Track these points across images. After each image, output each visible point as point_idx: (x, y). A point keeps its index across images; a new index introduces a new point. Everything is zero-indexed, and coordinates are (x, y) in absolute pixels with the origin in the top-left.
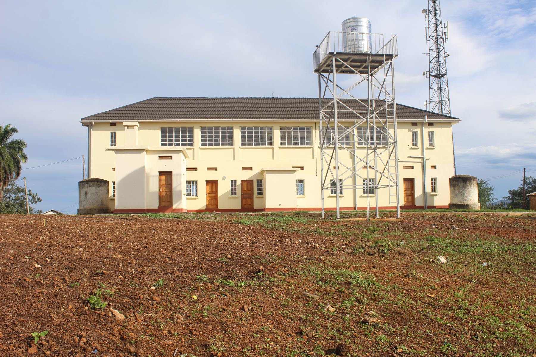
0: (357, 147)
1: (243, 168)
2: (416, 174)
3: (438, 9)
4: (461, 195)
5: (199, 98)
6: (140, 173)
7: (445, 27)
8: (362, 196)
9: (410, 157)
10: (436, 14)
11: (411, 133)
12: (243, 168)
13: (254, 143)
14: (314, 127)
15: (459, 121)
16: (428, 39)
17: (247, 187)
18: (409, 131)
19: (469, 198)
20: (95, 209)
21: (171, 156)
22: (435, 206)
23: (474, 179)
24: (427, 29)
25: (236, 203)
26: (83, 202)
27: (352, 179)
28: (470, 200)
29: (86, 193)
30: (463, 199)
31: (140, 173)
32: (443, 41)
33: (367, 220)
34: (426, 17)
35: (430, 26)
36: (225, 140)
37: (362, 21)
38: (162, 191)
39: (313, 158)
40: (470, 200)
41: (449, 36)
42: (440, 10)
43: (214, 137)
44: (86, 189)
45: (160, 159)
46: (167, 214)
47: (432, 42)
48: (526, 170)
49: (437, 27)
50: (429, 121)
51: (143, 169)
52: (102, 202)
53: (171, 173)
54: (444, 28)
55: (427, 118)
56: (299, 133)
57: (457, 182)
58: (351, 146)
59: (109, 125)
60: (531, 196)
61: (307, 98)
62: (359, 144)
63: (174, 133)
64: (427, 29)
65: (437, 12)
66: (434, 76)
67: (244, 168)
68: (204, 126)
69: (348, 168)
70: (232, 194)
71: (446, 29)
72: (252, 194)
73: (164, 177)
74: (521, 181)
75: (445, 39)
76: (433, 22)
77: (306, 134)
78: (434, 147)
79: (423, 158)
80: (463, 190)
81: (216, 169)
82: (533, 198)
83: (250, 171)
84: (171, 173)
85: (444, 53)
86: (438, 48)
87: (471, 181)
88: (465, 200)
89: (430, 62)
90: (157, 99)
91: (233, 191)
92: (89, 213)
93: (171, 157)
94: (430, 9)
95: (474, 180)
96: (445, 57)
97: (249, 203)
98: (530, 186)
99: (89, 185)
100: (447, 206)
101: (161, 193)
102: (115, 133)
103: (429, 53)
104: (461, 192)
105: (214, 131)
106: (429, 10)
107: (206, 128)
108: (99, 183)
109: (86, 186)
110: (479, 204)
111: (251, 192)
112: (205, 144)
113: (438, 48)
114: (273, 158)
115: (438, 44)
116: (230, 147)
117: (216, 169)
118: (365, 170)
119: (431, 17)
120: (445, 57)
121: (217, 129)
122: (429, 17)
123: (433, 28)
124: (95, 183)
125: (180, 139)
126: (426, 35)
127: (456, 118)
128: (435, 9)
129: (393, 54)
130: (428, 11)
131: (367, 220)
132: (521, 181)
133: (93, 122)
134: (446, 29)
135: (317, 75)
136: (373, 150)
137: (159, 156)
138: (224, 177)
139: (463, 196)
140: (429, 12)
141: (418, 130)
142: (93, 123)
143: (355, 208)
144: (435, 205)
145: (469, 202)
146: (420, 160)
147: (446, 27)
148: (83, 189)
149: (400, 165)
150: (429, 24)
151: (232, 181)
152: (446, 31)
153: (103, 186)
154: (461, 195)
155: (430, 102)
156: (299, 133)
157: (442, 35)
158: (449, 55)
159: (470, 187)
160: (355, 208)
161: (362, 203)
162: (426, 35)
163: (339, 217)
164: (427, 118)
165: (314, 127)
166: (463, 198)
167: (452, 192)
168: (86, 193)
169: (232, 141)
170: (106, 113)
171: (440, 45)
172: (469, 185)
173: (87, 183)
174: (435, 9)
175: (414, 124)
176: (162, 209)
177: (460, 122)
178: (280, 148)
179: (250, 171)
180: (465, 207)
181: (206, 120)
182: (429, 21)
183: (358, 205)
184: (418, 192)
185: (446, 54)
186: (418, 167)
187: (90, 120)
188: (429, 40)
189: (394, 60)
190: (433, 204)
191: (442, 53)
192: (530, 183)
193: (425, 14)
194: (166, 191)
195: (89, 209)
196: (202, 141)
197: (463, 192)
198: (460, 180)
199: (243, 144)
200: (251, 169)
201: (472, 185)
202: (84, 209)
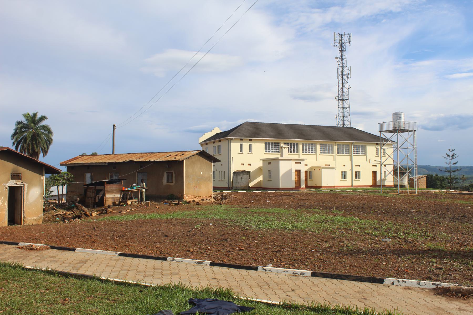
2: (377, 169)
8: (355, 180)
9: (375, 161)
10: (342, 60)
11: (376, 148)
20: (247, 187)
21: (300, 162)
24: (338, 69)
27: (351, 171)
29: (242, 178)
32: (347, 78)
39: (334, 160)
41: (351, 75)
42: (346, 58)
44: (241, 176)
47: (340, 77)
54: (348, 70)
55: (384, 142)
64: (338, 69)
66: (341, 100)
71: (350, 71)
75: (349, 77)
79: (381, 161)
85: (348, 86)
88: (404, 183)
89: (339, 91)
93: (300, 163)
96: (348, 89)
100: (393, 185)
109: (241, 174)
114: (317, 160)
116: (297, 153)
120: (348, 89)
123: (341, 69)
130: (338, 58)
133: (234, 138)
134: (350, 71)
140: (339, 59)
141: (379, 147)
143: (352, 186)
146: (379, 162)
147: (349, 69)
148: (239, 176)
150: (339, 67)
152: (350, 72)
155: (338, 116)
157: (347, 74)
158: (351, 87)
160: (352, 186)
162: (337, 73)
164: (384, 142)
168: (242, 178)
171: (344, 80)
173: (242, 173)
175: (377, 144)
184: (378, 179)
185: (349, 87)
186: (378, 165)
188: (339, 77)
191: (346, 86)
193: (337, 60)
202: (241, 187)
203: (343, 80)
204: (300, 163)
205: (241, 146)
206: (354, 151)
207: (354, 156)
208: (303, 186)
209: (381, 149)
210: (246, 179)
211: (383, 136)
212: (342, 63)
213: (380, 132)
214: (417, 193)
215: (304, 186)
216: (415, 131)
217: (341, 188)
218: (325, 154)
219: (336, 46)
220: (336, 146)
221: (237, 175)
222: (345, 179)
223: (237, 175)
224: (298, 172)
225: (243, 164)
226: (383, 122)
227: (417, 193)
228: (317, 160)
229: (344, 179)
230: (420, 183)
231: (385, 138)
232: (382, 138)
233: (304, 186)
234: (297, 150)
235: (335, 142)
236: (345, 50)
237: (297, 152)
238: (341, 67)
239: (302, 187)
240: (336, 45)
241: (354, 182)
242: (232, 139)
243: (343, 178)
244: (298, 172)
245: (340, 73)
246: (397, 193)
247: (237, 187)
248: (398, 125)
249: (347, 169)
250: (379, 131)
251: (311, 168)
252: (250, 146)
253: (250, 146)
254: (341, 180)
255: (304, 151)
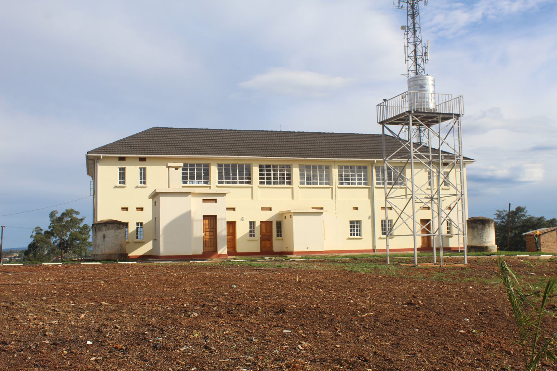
0: (375, 187)
1: (262, 208)
3: (417, 26)
4: (480, 237)
5: (203, 129)
6: (187, 217)
7: (425, 47)
8: (380, 238)
10: (415, 32)
11: (427, 172)
12: (262, 208)
13: (273, 182)
14: (333, 166)
15: (473, 162)
16: (407, 59)
17: (266, 229)
18: (426, 171)
19: (487, 240)
20: (115, 254)
21: (216, 200)
22: (451, 248)
23: (492, 221)
24: (406, 48)
25: (255, 246)
26: (100, 246)
27: (370, 220)
28: (489, 242)
29: (104, 237)
30: (482, 242)
31: (187, 217)
32: (423, 61)
33: (440, 266)
34: (405, 35)
35: (409, 44)
36: (243, 178)
37: (427, 80)
38: (206, 236)
39: (332, 198)
40: (489, 242)
41: (429, 56)
42: (420, 28)
43: (231, 174)
45: (203, 202)
46: (214, 260)
47: (411, 62)
48: (511, 206)
49: (415, 46)
50: (445, 161)
51: (189, 213)
52: (121, 246)
53: (215, 217)
54: (424, 48)
56: (318, 172)
57: (475, 224)
58: (370, 187)
59: (118, 159)
60: (529, 235)
61: (316, 133)
62: (378, 184)
63: (189, 170)
64: (406, 48)
65: (416, 29)
67: (263, 209)
68: (221, 162)
69: (409, 216)
70: (251, 236)
71: (426, 50)
72: (271, 236)
73: (207, 222)
74: (494, 214)
75: (426, 60)
76: (412, 40)
77: (325, 173)
78: (449, 188)
80: (482, 233)
81: (234, 209)
82: (529, 237)
83: (269, 212)
84: (215, 217)
86: (417, 70)
87: (489, 223)
88: (484, 242)
90: (157, 129)
91: (252, 234)
92: (95, 258)
93: (215, 201)
94: (409, 25)
95: (492, 222)
97: (268, 246)
98: (504, 221)
99: (107, 228)
101: (205, 238)
102: (124, 169)
103: (408, 75)
104: (480, 234)
105: (231, 168)
106: (408, 26)
107: (223, 165)
108: (118, 226)
109: (104, 228)
110: (496, 246)
111: (270, 234)
112: (222, 183)
113: (417, 70)
114: (293, 198)
115: (416, 64)
117: (234, 209)
118: (384, 211)
119: (410, 34)
121: (234, 166)
122: (408, 34)
123: (412, 48)
124: (114, 225)
125: (196, 176)
126: (405, 54)
127: (471, 158)
128: (414, 25)
129: (461, 113)
130: (407, 28)
131: (440, 266)
132: (494, 214)
133: (102, 155)
135: (381, 126)
136: (430, 200)
137: (203, 199)
138: (243, 218)
139: (482, 238)
140: (408, 29)
142: (102, 157)
143: (374, 251)
144: (450, 247)
145: (488, 244)
147: (426, 46)
148: (100, 232)
149: (417, 206)
150: (408, 43)
151: (251, 222)
152: (427, 51)
153: (122, 228)
154: (480, 237)
156: (318, 172)
157: (423, 55)
159: (489, 229)
160: (374, 251)
161: (381, 245)
162: (405, 54)
163: (416, 263)
165: (333, 166)
166: (482, 240)
167: (470, 234)
168: (104, 237)
169: (250, 179)
170: (111, 145)
171: (418, 65)
172: (487, 227)
173: (106, 225)
174: (414, 25)
176: (204, 256)
177: (474, 162)
178: (300, 188)
179: (269, 212)
180: (483, 249)
181: (225, 157)
182: (408, 39)
183: (378, 247)
187: (97, 153)
188: (408, 60)
189: (461, 119)
190: (449, 245)
192: (504, 217)
193: (403, 31)
194: (209, 236)
195: (109, 255)
196: (218, 179)
197: (482, 234)
198: (479, 222)
199: (261, 183)
200: (270, 209)
201: (491, 228)
202: (103, 254)
203: (416, 66)
204: (215, 201)
205: (122, 172)
206: (377, 180)
207: (377, 188)
208: (223, 250)
209: (439, 172)
210: (114, 237)
211: (387, 132)
212: (415, 37)
213: (382, 123)
214: (466, 263)
215: (223, 251)
216: (458, 116)
217: (327, 254)
218: (312, 186)
219: (402, 7)
220: (337, 170)
221: (96, 231)
222: (358, 237)
223: (96, 231)
224: (211, 220)
225: (126, 209)
226: (385, 100)
227: (466, 263)
228: (293, 198)
229: (357, 235)
230: (543, 242)
231: (391, 135)
232: (386, 135)
233: (223, 251)
234: (249, 178)
235: (335, 161)
236: (418, 14)
237: (248, 183)
238: (412, 43)
239: (219, 252)
240: (401, 6)
241: (377, 241)
242: (99, 158)
243: (354, 235)
244: (211, 220)
245: (410, 52)
246: (412, 264)
247: (94, 255)
248: (421, 105)
249: (363, 216)
250: (378, 122)
251: (281, 214)
252: (143, 172)
253: (143, 172)
254: (349, 239)
255: (265, 181)
